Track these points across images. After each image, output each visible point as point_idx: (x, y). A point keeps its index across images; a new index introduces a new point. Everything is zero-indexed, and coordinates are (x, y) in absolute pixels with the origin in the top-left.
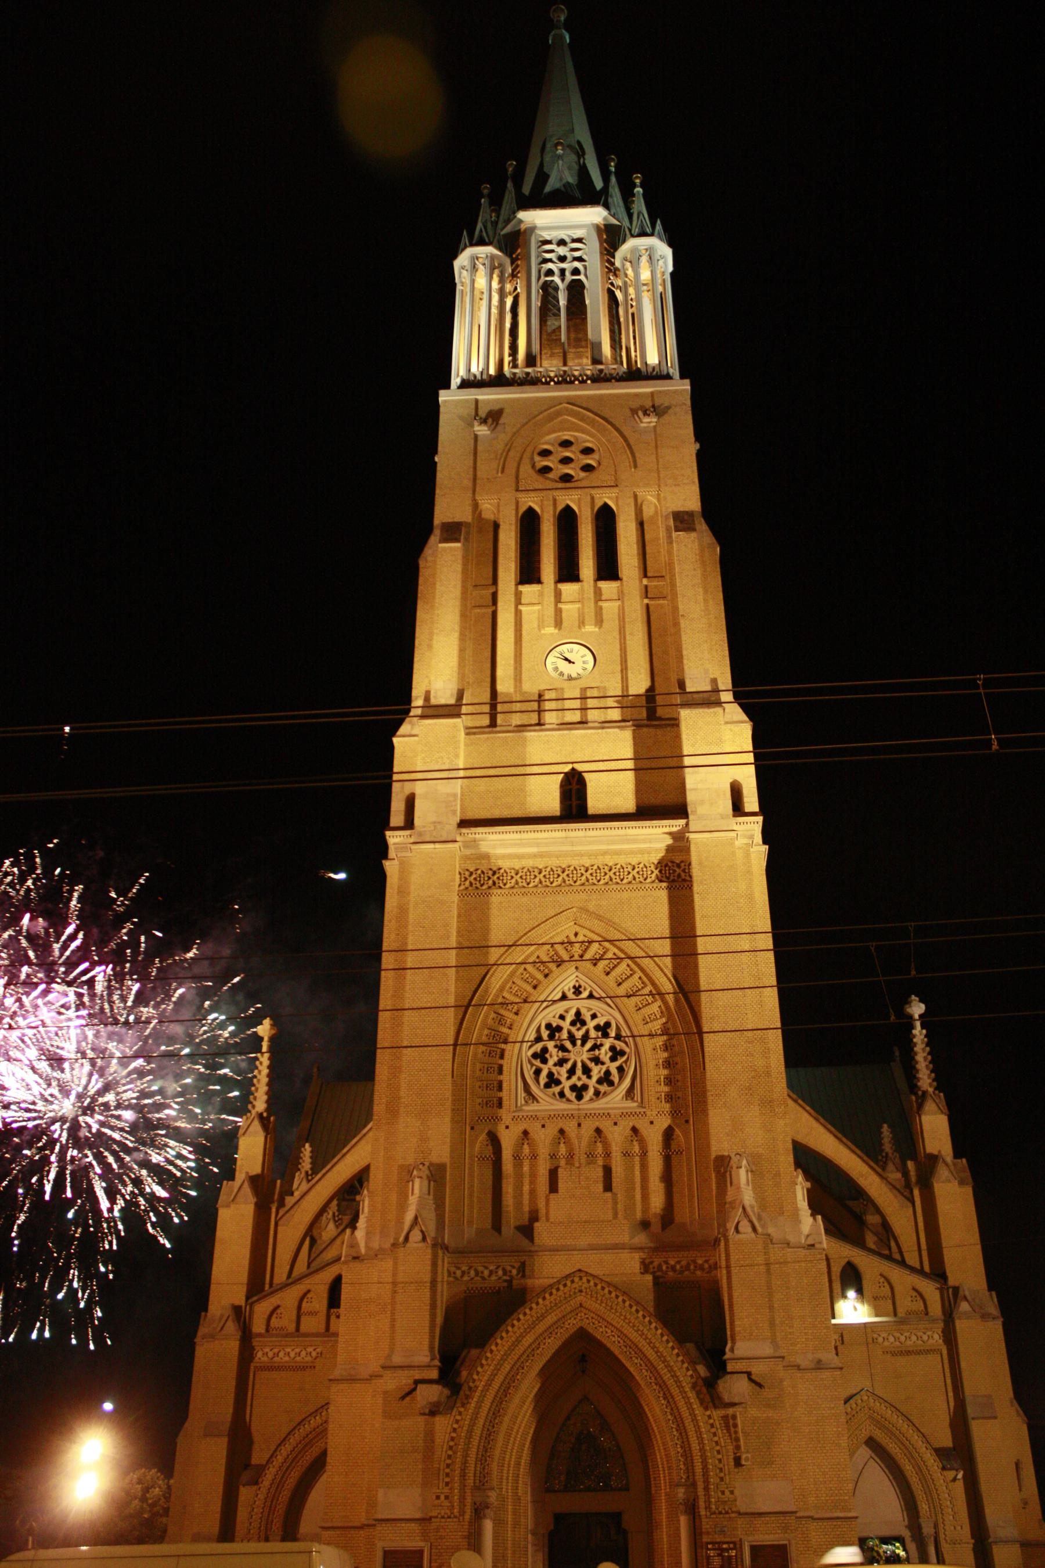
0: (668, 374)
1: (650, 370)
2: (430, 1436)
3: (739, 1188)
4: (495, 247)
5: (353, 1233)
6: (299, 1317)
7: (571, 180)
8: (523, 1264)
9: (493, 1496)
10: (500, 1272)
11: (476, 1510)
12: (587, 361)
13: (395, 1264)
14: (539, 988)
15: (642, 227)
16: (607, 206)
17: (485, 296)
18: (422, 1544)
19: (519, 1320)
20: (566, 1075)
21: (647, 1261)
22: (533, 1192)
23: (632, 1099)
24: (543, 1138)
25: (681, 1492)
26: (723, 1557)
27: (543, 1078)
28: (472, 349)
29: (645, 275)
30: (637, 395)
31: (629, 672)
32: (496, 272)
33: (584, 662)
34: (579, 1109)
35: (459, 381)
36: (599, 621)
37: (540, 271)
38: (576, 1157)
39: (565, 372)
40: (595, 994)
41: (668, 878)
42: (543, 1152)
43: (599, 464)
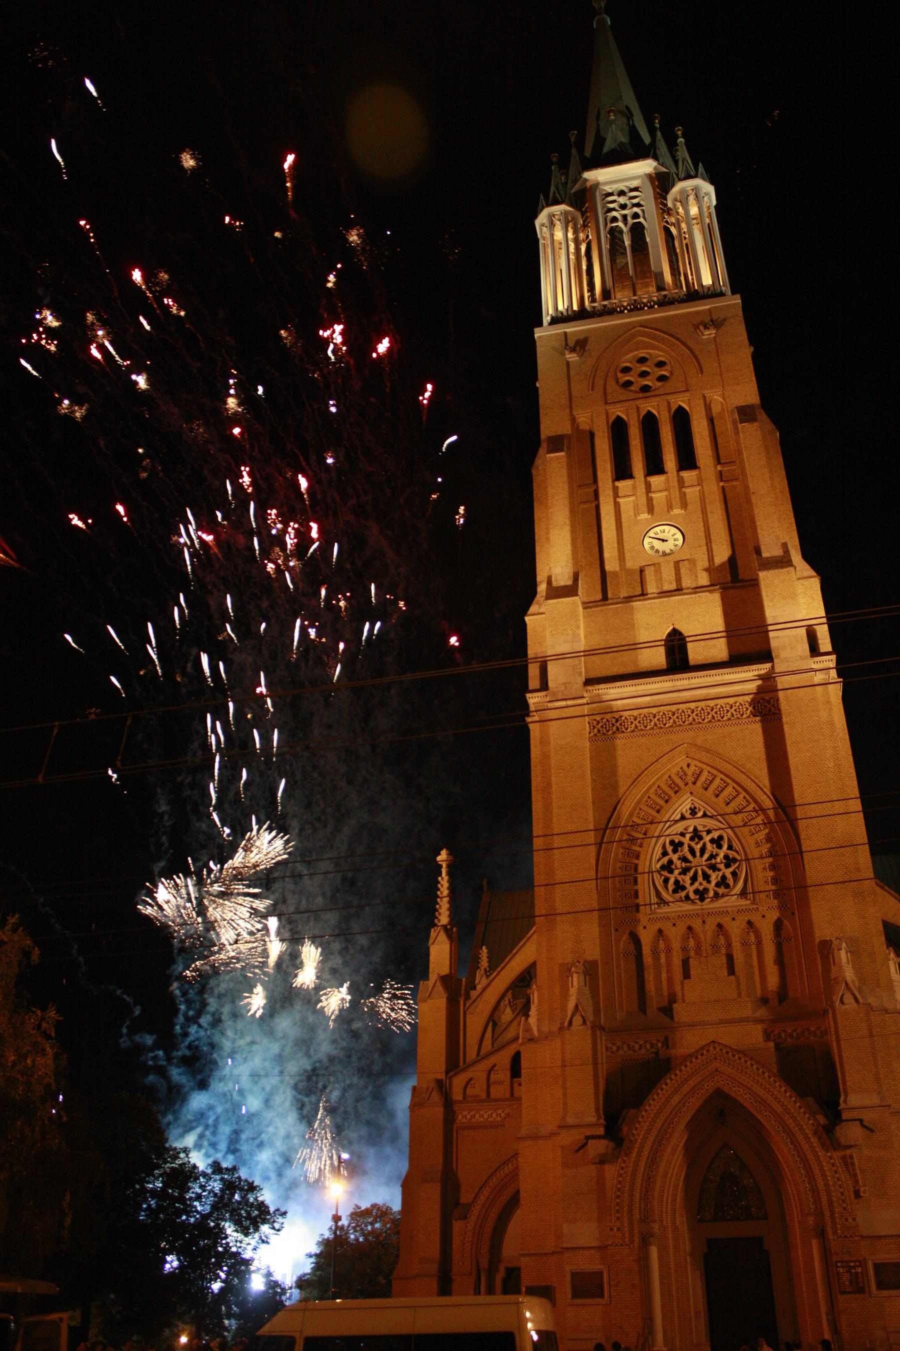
0: (721, 291)
1: (706, 290)
2: (601, 1181)
3: (841, 967)
4: (567, 205)
5: (526, 1020)
6: (488, 1086)
7: (623, 140)
8: (667, 1038)
9: (656, 1227)
10: (648, 1046)
11: (643, 1239)
12: (652, 289)
13: (563, 1043)
14: (662, 811)
15: (687, 171)
16: (656, 158)
17: (564, 246)
18: (602, 1267)
19: (666, 1084)
20: (689, 882)
21: (768, 1031)
22: (670, 980)
23: (746, 898)
24: (675, 934)
25: (811, 1220)
26: (851, 1273)
27: (671, 886)
28: (557, 292)
29: (694, 211)
30: (697, 313)
31: (713, 544)
32: (570, 225)
33: (675, 540)
34: (702, 909)
35: (549, 318)
36: (684, 505)
37: (606, 219)
38: (703, 948)
39: (635, 300)
40: (709, 814)
41: (761, 713)
42: (676, 945)
43: (672, 373)
